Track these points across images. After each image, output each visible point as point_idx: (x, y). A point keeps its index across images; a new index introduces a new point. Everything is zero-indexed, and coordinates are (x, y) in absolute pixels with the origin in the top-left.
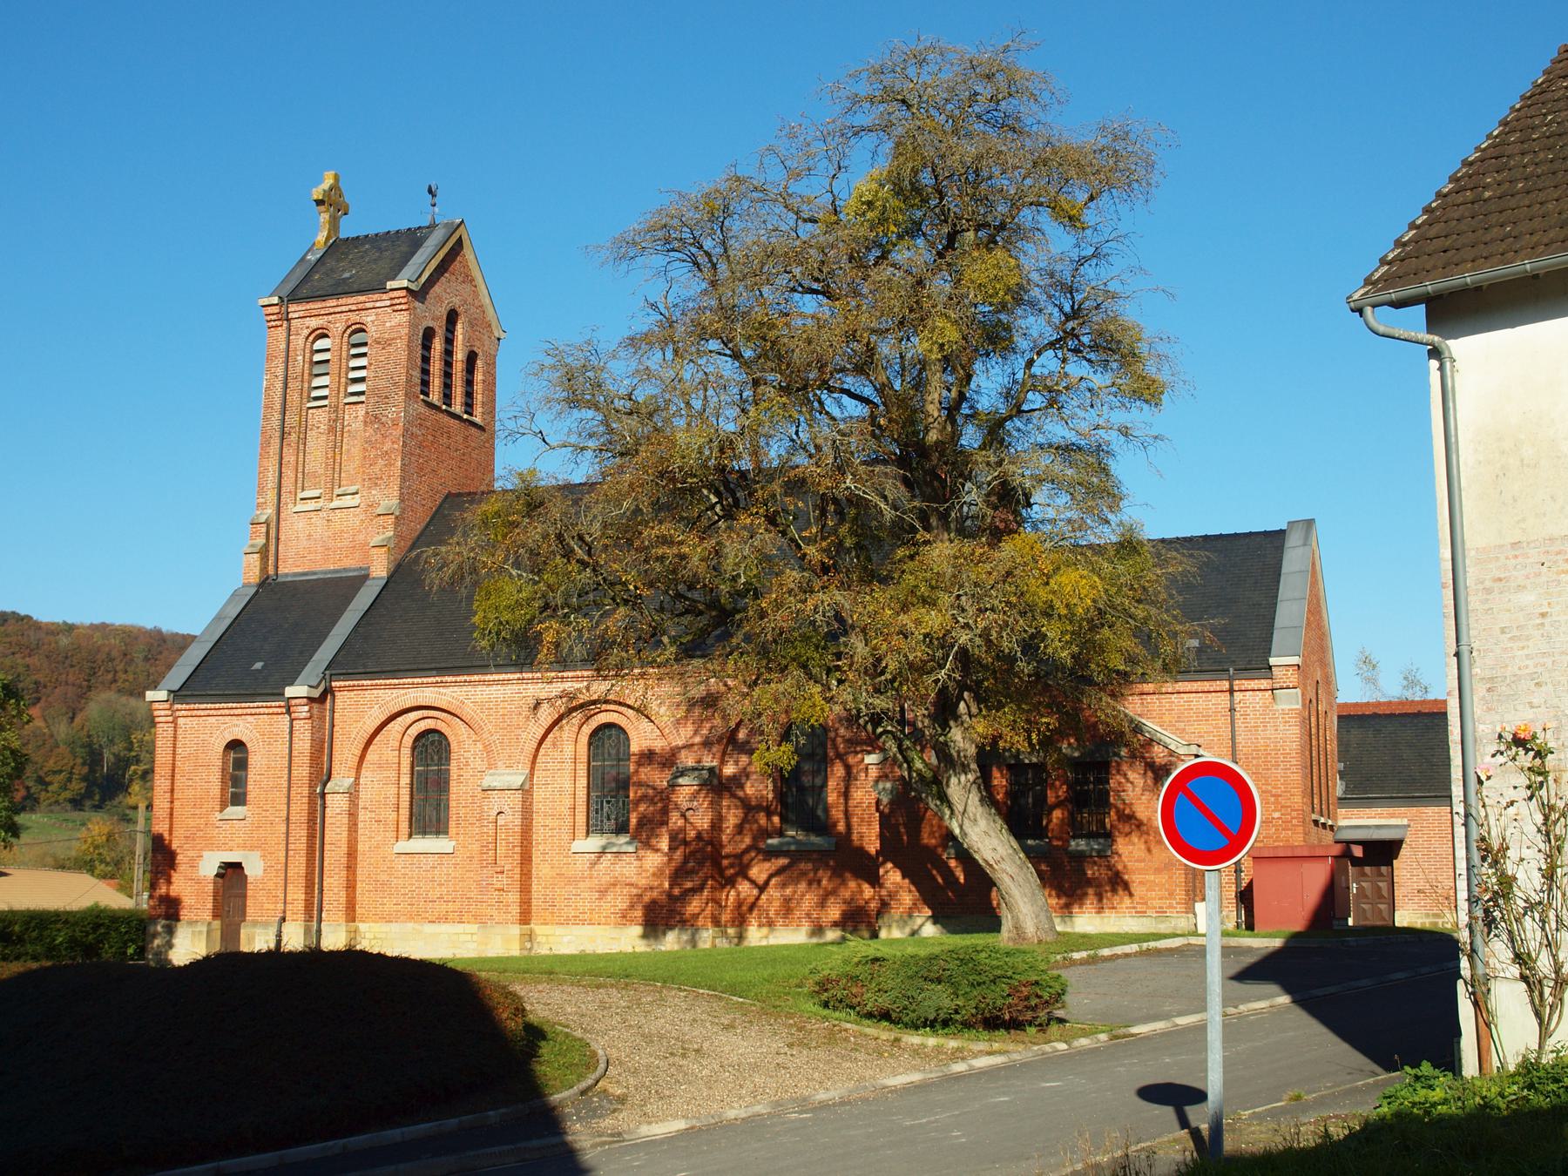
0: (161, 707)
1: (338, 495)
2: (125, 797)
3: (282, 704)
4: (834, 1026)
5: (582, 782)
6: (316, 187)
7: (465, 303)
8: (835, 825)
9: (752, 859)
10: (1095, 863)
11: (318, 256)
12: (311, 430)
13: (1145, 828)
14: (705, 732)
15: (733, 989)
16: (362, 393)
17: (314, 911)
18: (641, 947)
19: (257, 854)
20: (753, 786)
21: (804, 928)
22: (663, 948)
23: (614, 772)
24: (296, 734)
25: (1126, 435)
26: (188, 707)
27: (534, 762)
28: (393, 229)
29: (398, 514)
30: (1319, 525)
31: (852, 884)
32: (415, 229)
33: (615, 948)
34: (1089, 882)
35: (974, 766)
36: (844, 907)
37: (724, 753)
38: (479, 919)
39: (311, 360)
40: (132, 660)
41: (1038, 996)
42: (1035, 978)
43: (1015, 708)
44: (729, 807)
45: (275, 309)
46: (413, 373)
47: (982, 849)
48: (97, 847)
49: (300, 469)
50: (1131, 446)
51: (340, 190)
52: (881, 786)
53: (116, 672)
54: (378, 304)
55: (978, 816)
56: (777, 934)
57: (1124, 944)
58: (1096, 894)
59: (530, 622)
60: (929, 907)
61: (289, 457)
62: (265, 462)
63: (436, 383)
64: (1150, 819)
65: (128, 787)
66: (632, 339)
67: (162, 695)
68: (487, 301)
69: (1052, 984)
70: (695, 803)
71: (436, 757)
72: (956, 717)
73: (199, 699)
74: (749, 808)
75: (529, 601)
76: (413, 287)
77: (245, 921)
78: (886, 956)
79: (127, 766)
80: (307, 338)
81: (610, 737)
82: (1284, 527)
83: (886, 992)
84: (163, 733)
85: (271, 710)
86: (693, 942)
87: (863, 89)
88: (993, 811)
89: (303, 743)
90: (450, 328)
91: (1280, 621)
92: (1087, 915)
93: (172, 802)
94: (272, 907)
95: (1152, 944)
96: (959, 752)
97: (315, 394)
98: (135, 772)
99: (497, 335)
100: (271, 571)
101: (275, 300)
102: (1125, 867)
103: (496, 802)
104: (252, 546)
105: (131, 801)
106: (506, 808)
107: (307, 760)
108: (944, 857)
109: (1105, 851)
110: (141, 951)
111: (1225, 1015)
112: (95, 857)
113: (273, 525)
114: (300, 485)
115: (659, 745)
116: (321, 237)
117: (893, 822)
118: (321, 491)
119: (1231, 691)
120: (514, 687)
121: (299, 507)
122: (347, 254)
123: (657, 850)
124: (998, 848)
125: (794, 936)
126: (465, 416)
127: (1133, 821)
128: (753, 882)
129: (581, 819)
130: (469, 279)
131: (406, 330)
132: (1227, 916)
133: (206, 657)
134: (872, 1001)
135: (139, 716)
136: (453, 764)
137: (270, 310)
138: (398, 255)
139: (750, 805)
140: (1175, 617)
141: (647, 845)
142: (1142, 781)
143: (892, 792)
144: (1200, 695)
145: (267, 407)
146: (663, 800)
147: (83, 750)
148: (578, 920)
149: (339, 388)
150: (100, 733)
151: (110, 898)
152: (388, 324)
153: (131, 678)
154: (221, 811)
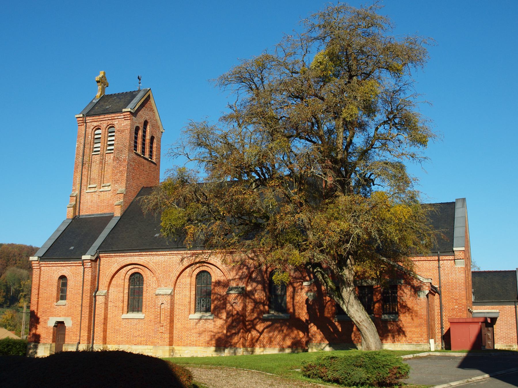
0: (35, 263)
1: (103, 187)
2: (18, 304)
3: (81, 262)
4: (314, 385)
5: (193, 292)
6: (97, 76)
7: (151, 118)
8: (289, 309)
9: (258, 322)
10: (392, 324)
11: (97, 101)
12: (93, 163)
13: (411, 311)
14: (240, 274)
15: (266, 370)
16: (112, 150)
17: (91, 339)
18: (215, 355)
20: (258, 295)
21: (277, 348)
22: (223, 355)
23: (205, 289)
24: (86, 273)
25: (413, 157)
26: (45, 263)
27: (175, 285)
28: (125, 91)
29: (125, 193)
30: (467, 201)
31: (296, 332)
32: (133, 92)
33: (205, 355)
34: (389, 331)
35: (352, 284)
36: (292, 340)
37: (247, 282)
38: (153, 343)
39: (94, 137)
40: (22, 256)
41: (399, 373)
42: (399, 366)
43: (370, 261)
44: (249, 302)
45: (81, 119)
46: (132, 142)
47: (355, 317)
48: (8, 320)
49: (89, 177)
50: (415, 161)
51: (105, 78)
52: (309, 294)
53: (16, 260)
54: (119, 117)
55: (354, 304)
56: (267, 350)
57: (407, 354)
58: (392, 336)
59: (184, 224)
60: (328, 341)
61: (85, 172)
62: (76, 174)
63: (139, 146)
64: (413, 307)
65: (19, 300)
66: (224, 117)
67: (36, 258)
68: (158, 118)
69: (405, 368)
70: (237, 301)
71: (138, 283)
72: (346, 265)
73: (50, 260)
74: (256, 303)
75: (183, 217)
76: (132, 111)
77: (64, 343)
78: (337, 356)
79: (19, 293)
80: (93, 129)
81: (204, 276)
82: (454, 201)
83: (337, 371)
84: (36, 272)
85: (76, 264)
86: (235, 353)
87: (316, 22)
88: (359, 302)
89: (88, 277)
90: (145, 127)
91: (456, 235)
92: (389, 344)
93: (38, 298)
94: (75, 338)
95: (418, 355)
96: (347, 279)
97: (95, 150)
98: (22, 295)
99: (161, 131)
100: (77, 214)
101: (81, 116)
102: (403, 325)
103: (161, 299)
104: (70, 205)
105: (20, 305)
106: (164, 302)
107: (89, 283)
108: (334, 321)
109: (395, 319)
110: (25, 354)
112: (7, 324)
113: (78, 197)
114: (89, 183)
115: (222, 279)
116: (98, 94)
117: (314, 308)
118: (96, 185)
119: (439, 260)
120: (168, 256)
121: (88, 191)
122: (108, 100)
123: (221, 319)
124: (361, 317)
125: (273, 351)
126: (150, 159)
127: (406, 308)
128: (258, 331)
129: (193, 306)
130: (152, 110)
131: (129, 127)
132: (438, 345)
133: (52, 244)
134: (330, 375)
135: (24, 275)
136: (145, 285)
137: (79, 119)
138: (127, 100)
139: (257, 301)
140: (430, 228)
141: (217, 316)
142: (410, 293)
143: (313, 296)
144: (427, 261)
145: (77, 154)
146: (224, 300)
147: (4, 287)
148: (191, 345)
149: (104, 148)
150: (10, 281)
151: (12, 336)
152: (123, 125)
153: (21, 262)
154: (57, 302)
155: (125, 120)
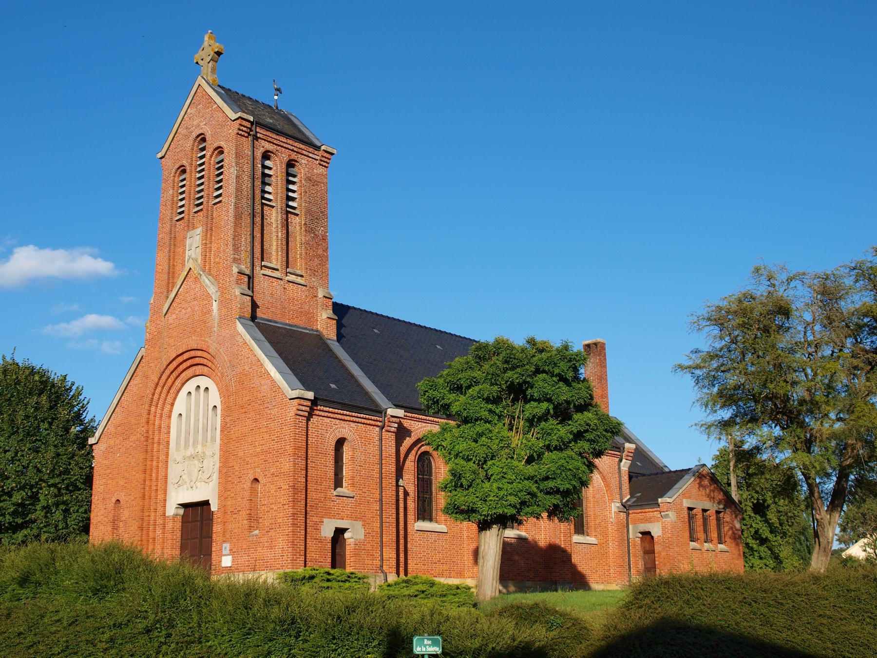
19: (359, 524)
54: (311, 155)
85: (369, 422)
137: (244, 123)
155: (320, 165)
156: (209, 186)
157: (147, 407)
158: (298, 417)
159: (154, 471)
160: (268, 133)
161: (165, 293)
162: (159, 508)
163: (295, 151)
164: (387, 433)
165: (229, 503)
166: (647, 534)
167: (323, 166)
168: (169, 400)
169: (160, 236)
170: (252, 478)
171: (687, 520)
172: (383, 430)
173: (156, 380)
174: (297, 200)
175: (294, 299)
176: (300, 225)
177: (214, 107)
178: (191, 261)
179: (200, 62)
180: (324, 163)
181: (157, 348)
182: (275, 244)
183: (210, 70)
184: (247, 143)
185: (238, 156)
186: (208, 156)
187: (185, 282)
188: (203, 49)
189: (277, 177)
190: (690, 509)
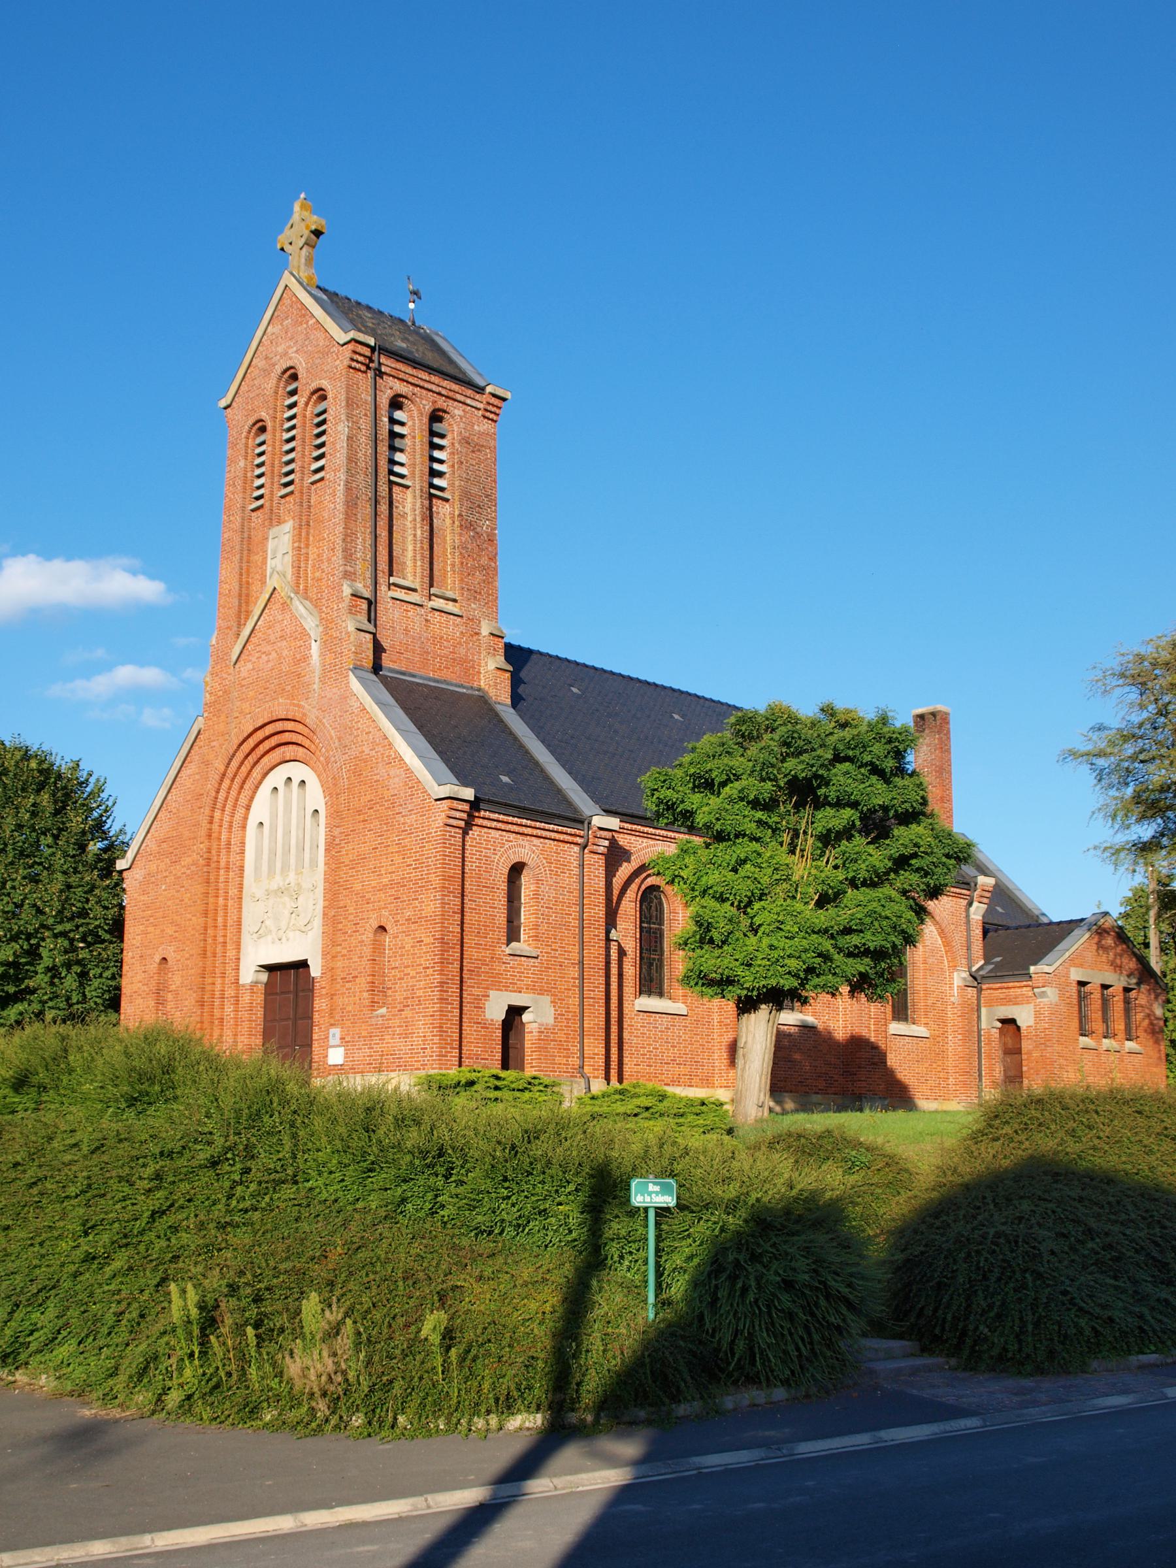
19: (546, 999)
85: (562, 837)
111: (646, 1209)
137: (360, 349)
155: (485, 417)
156: (304, 452)
157: (207, 811)
158: (448, 828)
159: (221, 913)
160: (400, 366)
161: (235, 629)
162: (230, 973)
163: (443, 395)
164: (592, 855)
165: (339, 964)
166: (1009, 1022)
167: (489, 419)
168: (243, 800)
169: (226, 536)
170: (375, 925)
171: (1075, 1002)
172: (586, 851)
173: (222, 768)
174: (447, 475)
175: (441, 638)
176: (452, 518)
177: (310, 322)
178: (275, 576)
179: (287, 248)
180: (491, 414)
181: (223, 717)
182: (410, 548)
183: (303, 260)
184: (364, 381)
185: (350, 403)
186: (301, 404)
187: (266, 611)
188: (292, 226)
189: (414, 437)
190: (1082, 984)
